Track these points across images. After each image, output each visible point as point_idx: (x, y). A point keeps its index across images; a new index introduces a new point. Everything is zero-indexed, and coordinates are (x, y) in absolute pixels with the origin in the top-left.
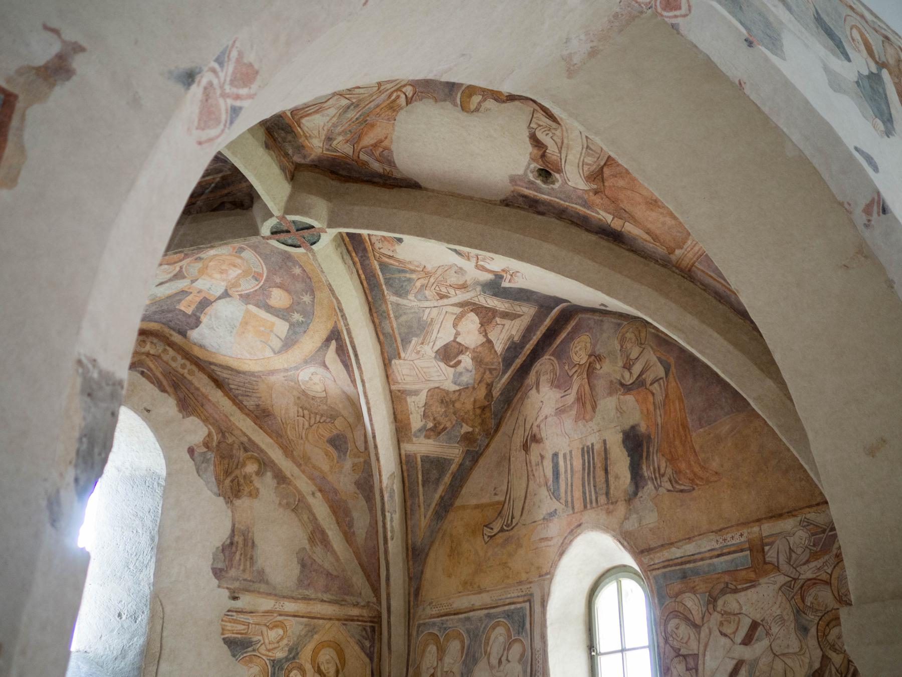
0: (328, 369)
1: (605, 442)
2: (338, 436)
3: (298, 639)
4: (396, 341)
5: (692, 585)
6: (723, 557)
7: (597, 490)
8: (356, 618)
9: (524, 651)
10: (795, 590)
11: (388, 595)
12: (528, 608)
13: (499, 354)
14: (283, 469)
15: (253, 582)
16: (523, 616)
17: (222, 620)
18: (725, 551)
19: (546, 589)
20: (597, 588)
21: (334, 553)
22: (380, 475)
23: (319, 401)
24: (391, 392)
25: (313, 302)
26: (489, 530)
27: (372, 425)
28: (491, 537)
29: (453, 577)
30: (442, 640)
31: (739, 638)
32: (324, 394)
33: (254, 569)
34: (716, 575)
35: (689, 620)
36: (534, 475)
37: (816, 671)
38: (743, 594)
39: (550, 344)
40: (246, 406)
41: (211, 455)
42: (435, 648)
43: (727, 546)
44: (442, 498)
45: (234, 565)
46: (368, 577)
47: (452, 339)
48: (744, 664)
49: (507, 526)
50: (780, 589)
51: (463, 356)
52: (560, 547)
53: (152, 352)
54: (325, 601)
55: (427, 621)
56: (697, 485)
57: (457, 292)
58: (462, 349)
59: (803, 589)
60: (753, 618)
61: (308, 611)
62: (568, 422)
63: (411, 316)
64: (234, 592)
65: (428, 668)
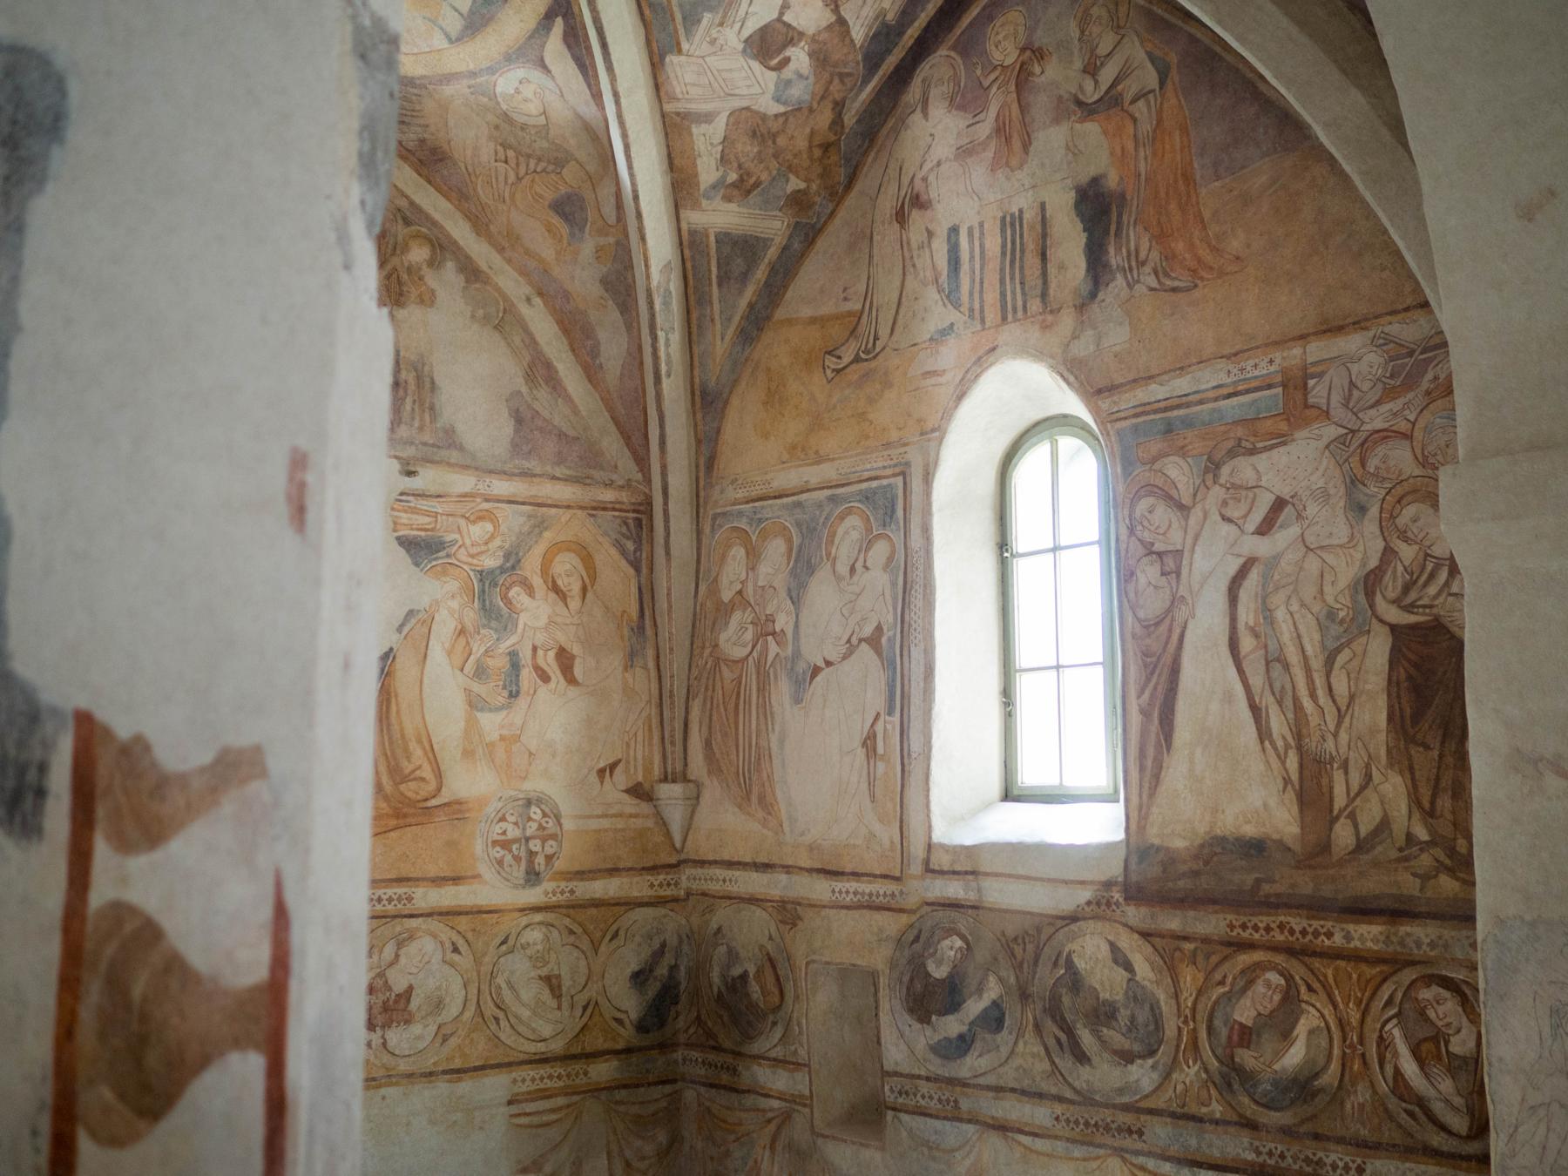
0: (549, 72)
1: (1043, 206)
2: (569, 197)
3: (518, 538)
4: (673, 20)
5: (1180, 443)
6: (1236, 399)
7: (1026, 289)
8: (610, 506)
9: (893, 552)
10: (1352, 449)
11: (664, 468)
12: (901, 485)
13: (858, 46)
14: (474, 255)
15: (439, 447)
16: (893, 500)
17: (393, 509)
18: (1240, 388)
19: (932, 454)
20: (1017, 451)
21: (568, 399)
22: (647, 266)
23: (533, 132)
24: (663, 116)
26: (834, 359)
27: (632, 175)
28: (838, 371)
29: (773, 438)
30: (754, 538)
31: (1251, 526)
32: (542, 120)
33: (438, 426)
34: (1223, 428)
35: (1171, 498)
36: (914, 266)
37: (1372, 571)
38: (1264, 456)
39: (950, 29)
42: (742, 551)
43: (1245, 380)
44: (751, 306)
45: (403, 420)
46: (627, 439)
47: (775, 15)
48: (1256, 564)
49: (867, 352)
50: (1327, 447)
51: (793, 49)
52: (958, 385)
54: (558, 479)
55: (728, 509)
56: (1202, 279)
58: (791, 36)
59: (1366, 446)
60: (1278, 494)
61: (531, 493)
62: (979, 172)
64: (408, 464)
65: (732, 583)
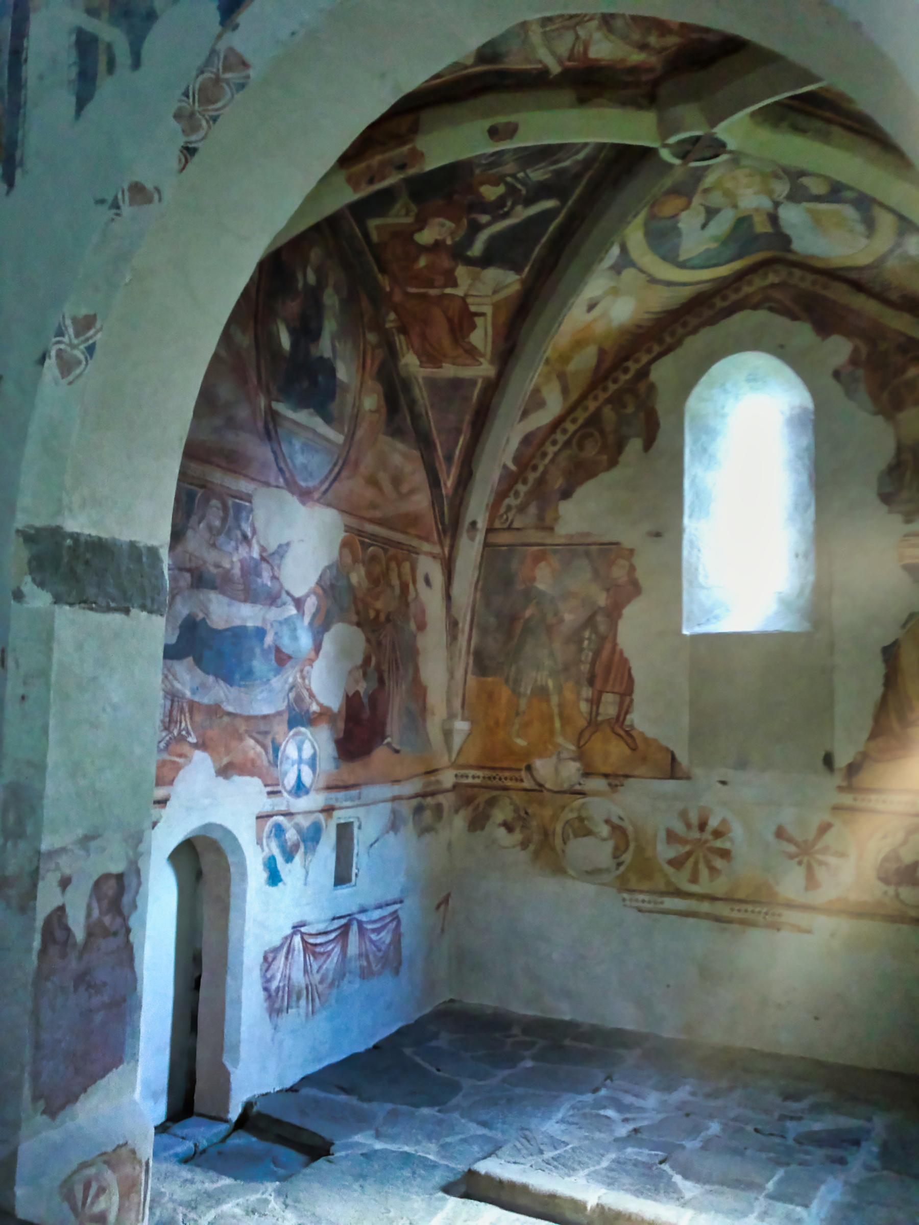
41: (860, 372)
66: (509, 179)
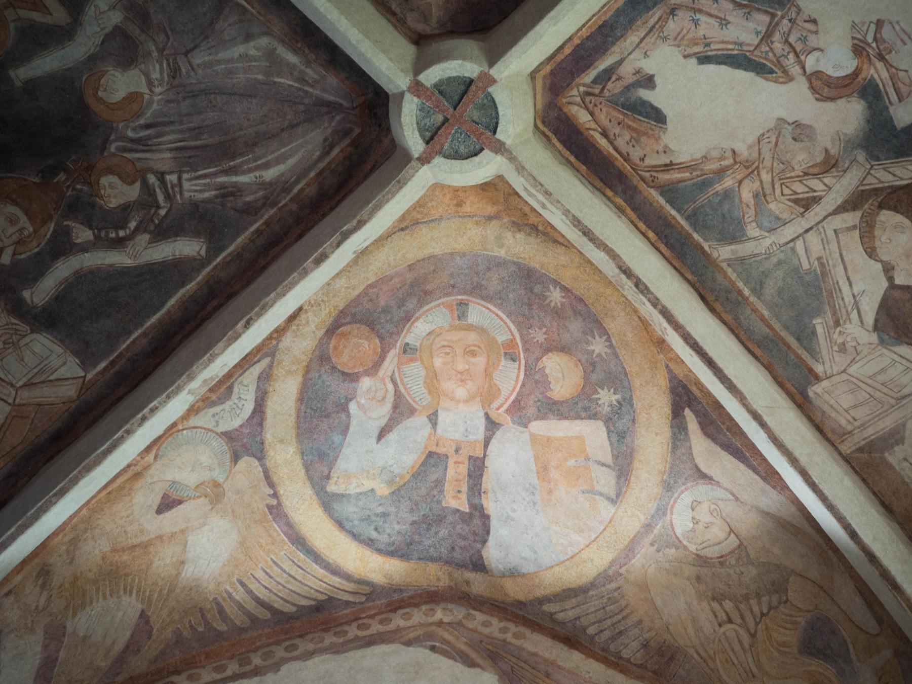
0: (711, 479)
4: (789, 347)
25: (611, 346)
32: (733, 541)
40: (628, 661)
47: (885, 284)
53: (446, 619)
57: (827, 180)
63: (779, 274)
66: (152, 179)
